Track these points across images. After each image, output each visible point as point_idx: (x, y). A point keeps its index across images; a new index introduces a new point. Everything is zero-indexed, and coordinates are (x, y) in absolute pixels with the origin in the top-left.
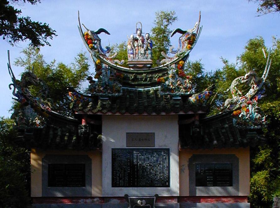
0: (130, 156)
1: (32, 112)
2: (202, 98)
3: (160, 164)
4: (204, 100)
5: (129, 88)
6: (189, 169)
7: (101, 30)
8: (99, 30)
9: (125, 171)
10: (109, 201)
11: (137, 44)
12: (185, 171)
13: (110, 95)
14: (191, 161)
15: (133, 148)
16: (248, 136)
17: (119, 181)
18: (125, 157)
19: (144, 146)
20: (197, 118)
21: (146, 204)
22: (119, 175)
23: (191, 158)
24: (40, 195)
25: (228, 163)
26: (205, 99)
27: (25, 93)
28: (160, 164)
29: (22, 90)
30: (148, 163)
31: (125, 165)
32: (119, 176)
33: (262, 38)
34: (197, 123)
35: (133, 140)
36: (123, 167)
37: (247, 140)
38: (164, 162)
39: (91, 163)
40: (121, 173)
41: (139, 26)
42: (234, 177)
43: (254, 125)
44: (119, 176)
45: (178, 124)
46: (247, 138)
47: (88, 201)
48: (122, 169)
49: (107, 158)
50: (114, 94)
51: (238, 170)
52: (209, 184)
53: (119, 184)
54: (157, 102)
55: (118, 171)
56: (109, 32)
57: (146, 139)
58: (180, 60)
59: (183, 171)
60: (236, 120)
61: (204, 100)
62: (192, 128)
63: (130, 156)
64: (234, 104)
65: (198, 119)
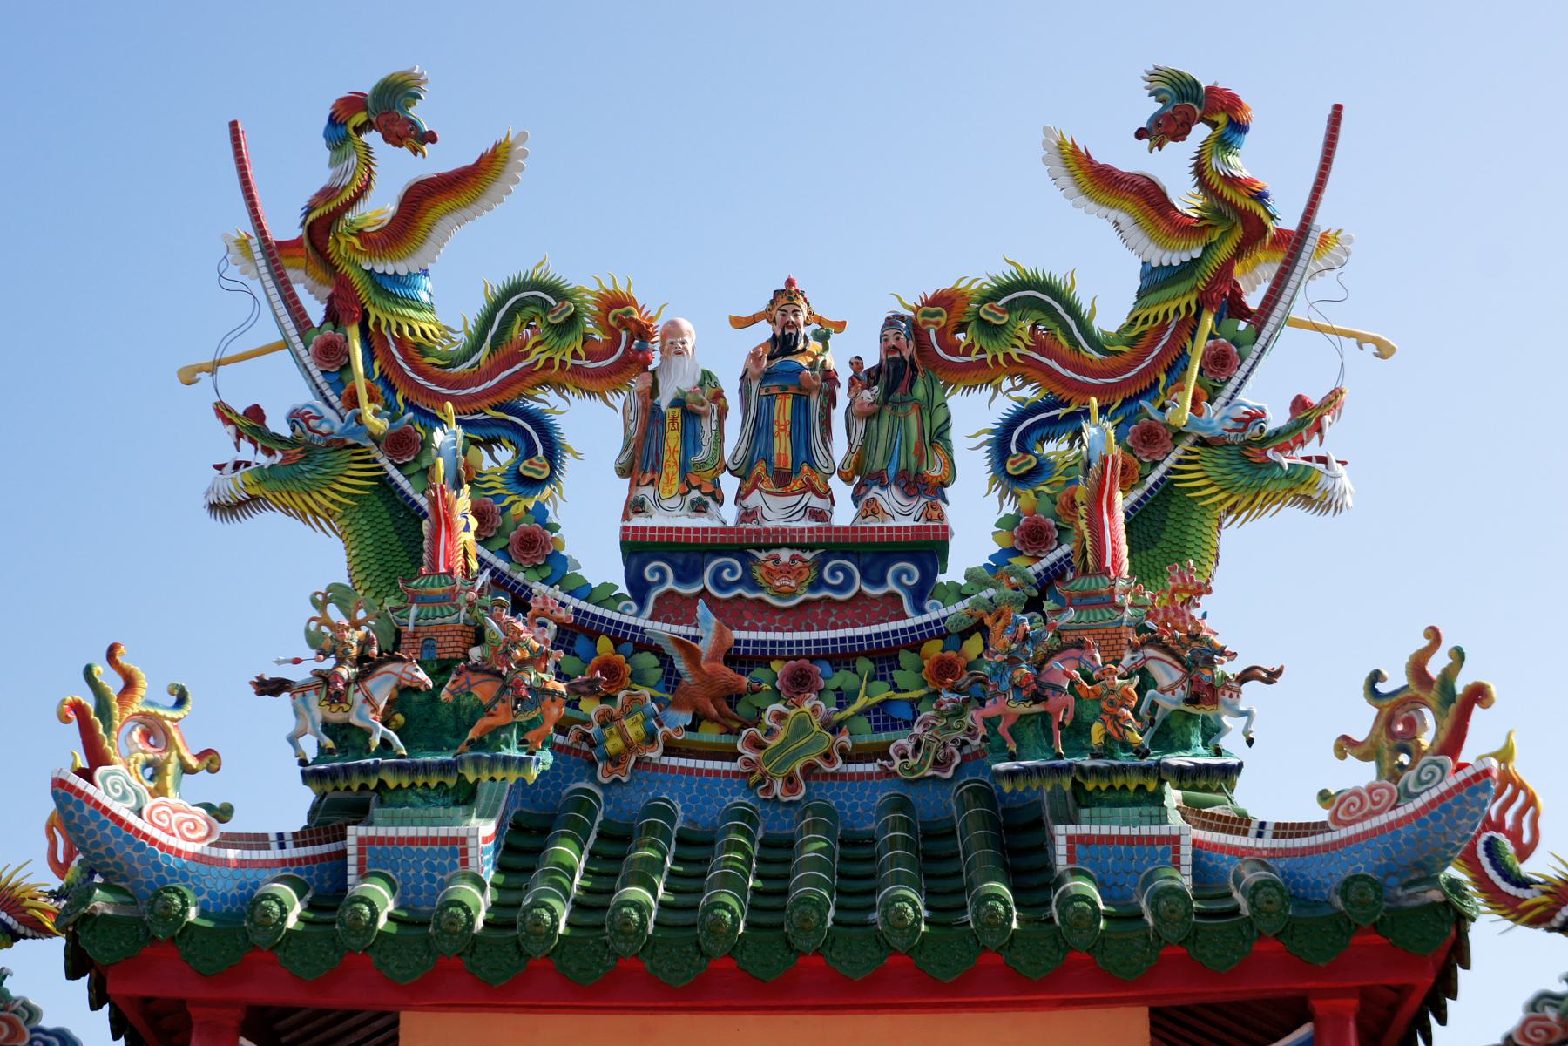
54: (814, 847)
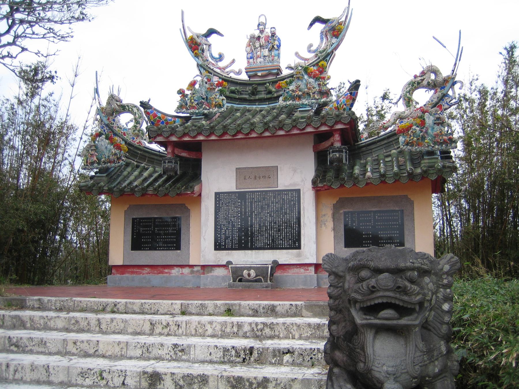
0: (241, 203)
1: (106, 145)
2: (341, 104)
3: (286, 213)
4: (345, 107)
5: (247, 106)
6: (333, 221)
7: (211, 32)
8: (208, 31)
9: (233, 226)
10: (211, 272)
11: (259, 44)
12: (327, 224)
13: (206, 111)
14: (336, 208)
15: (243, 190)
16: (424, 163)
17: (225, 241)
18: (234, 204)
19: (259, 186)
20: (337, 137)
21: (256, 276)
22: (225, 231)
23: (336, 204)
24: (120, 263)
25: (397, 209)
26: (345, 105)
27: (111, 124)
28: (286, 213)
29: (108, 119)
30: (268, 213)
31: (234, 217)
32: (225, 234)
33: (495, 88)
34: (338, 145)
35: (245, 179)
36: (231, 220)
37: (421, 168)
38: (292, 211)
39: (189, 216)
40: (227, 229)
41: (262, 20)
42: (406, 232)
43: (433, 144)
44: (225, 234)
45: (314, 151)
46: (422, 165)
47: (186, 270)
48: (229, 223)
49: (208, 206)
50: (211, 110)
51: (413, 220)
52: (365, 244)
53: (225, 245)
55: (224, 225)
56: (221, 32)
57: (264, 177)
58: (321, 61)
59: (325, 224)
60: (403, 139)
61: (345, 107)
62: (330, 154)
63: (241, 203)
64: (405, 118)
65: (338, 139)
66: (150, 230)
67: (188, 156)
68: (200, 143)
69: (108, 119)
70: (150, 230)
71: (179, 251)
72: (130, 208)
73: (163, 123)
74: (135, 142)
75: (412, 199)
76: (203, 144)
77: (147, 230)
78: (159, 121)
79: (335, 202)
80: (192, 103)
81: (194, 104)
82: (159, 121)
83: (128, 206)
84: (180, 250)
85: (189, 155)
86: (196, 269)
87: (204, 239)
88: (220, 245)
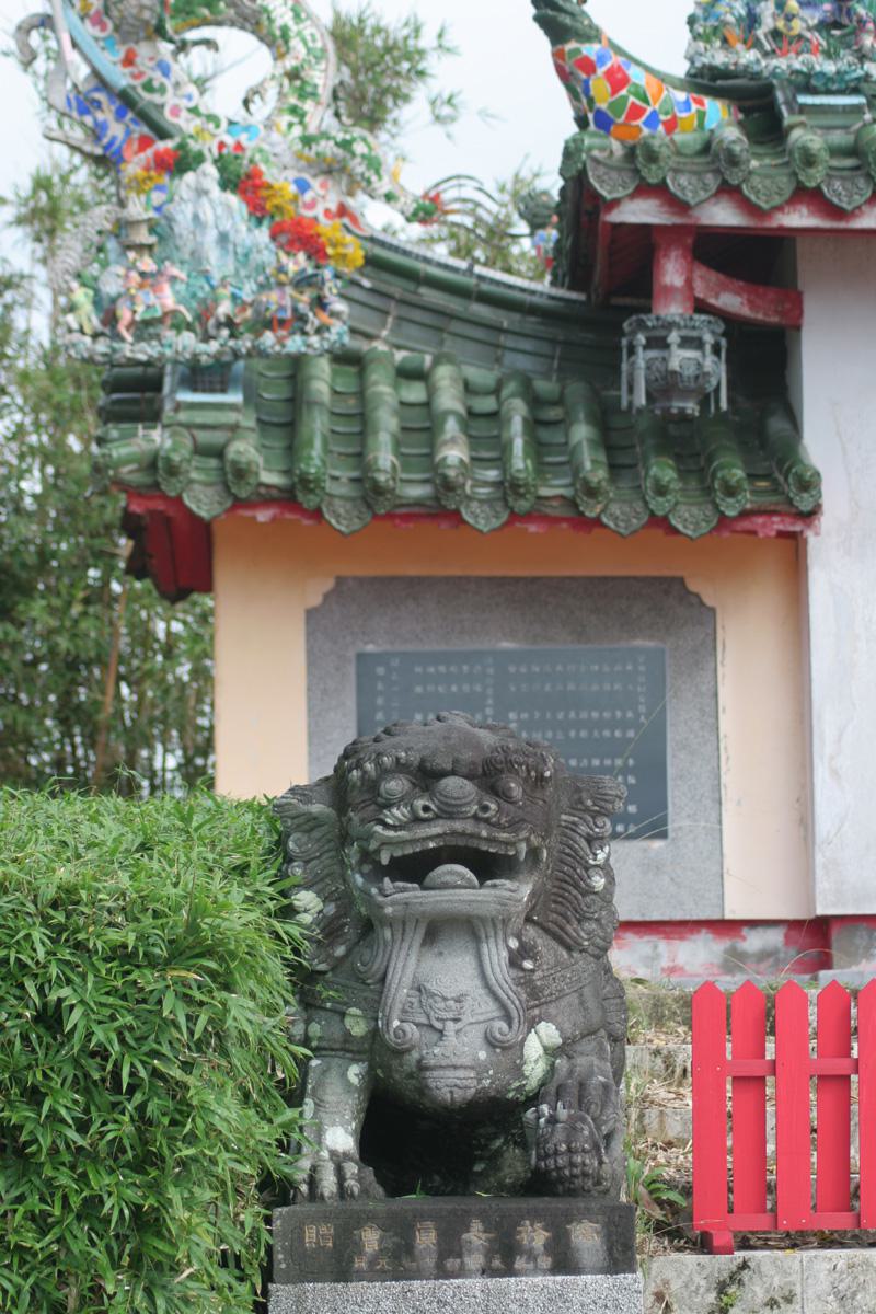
27: (148, 87)
29: (129, 61)
39: (709, 646)
66: (624, 725)
67: (746, 312)
68: (788, 237)
69: (129, 61)
70: (624, 725)
71: (657, 844)
72: (341, 590)
73: (652, 121)
74: (311, 205)
75: (709, 601)
76: (802, 247)
77: (613, 724)
78: (636, 112)
79: (315, 600)
80: (789, 18)
81: (798, 26)
82: (636, 112)
83: (329, 584)
84: (663, 835)
85: (751, 303)
86: (754, 941)
87: (835, 773)
88: (653, 826)
